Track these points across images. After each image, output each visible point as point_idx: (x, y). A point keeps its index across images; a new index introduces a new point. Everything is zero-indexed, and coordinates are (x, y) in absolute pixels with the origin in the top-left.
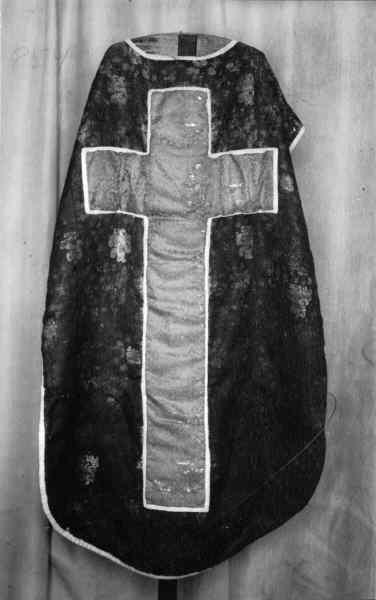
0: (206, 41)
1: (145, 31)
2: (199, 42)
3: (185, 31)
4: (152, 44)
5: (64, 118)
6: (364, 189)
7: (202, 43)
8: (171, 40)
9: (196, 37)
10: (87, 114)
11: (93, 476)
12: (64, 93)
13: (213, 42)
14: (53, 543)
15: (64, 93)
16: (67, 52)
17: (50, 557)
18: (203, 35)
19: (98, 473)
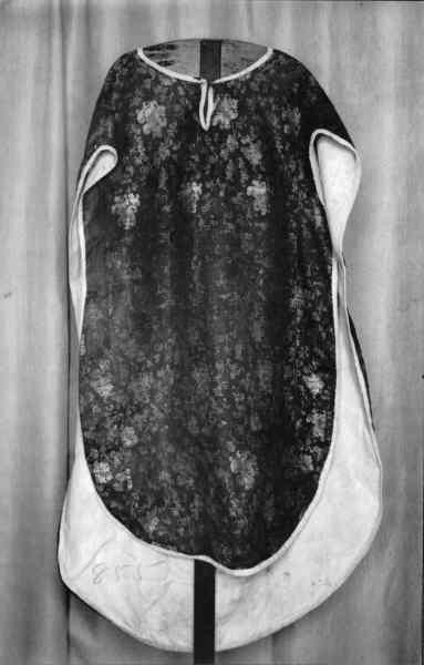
0: (231, 48)
1: (161, 38)
2: (223, 48)
3: (207, 37)
4: (169, 51)
5: (70, 89)
6: (313, 584)
7: (227, 50)
8: (192, 47)
9: (219, 43)
10: (93, 275)
11: (134, 217)
12: (70, 107)
13: (247, 52)
14: (71, 613)
15: (70, 107)
16: (77, 214)
17: (68, 638)
18: (227, 40)
19: (140, 214)
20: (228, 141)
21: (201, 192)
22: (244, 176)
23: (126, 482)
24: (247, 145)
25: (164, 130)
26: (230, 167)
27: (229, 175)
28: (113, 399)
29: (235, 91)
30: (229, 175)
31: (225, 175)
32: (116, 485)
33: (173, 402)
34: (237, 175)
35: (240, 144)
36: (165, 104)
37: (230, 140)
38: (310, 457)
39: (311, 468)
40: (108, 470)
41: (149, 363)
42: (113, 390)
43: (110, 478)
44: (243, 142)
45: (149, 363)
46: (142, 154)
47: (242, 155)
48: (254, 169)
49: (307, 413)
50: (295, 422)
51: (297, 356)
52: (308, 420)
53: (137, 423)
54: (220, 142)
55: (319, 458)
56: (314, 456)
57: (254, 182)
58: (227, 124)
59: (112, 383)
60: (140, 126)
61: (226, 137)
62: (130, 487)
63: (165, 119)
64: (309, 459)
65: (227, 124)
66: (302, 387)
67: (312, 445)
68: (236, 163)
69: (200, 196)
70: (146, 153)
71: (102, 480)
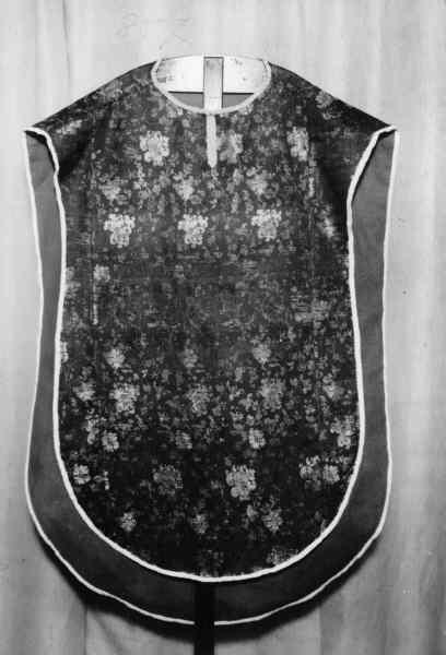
20: (235, 175)
21: (133, 226)
22: (176, 211)
23: (103, 483)
24: (252, 177)
25: (166, 159)
26: (236, 200)
27: (234, 208)
28: (95, 403)
29: (239, 127)
30: (234, 208)
31: (231, 209)
32: (93, 486)
33: (253, 413)
34: (242, 206)
35: (173, 181)
36: (241, 133)
37: (236, 174)
38: (336, 468)
39: (337, 478)
40: (86, 472)
41: (136, 376)
42: (95, 395)
43: (88, 480)
44: (248, 174)
45: (136, 376)
46: (141, 180)
47: (174, 191)
48: (185, 203)
49: (331, 422)
50: (319, 434)
51: (317, 367)
52: (332, 431)
53: (121, 430)
54: (227, 177)
55: (344, 469)
56: (340, 466)
57: (185, 216)
58: (234, 159)
59: (94, 389)
60: (142, 153)
61: (233, 171)
62: (107, 487)
63: (168, 150)
64: (334, 470)
65: (234, 159)
66: (323, 398)
67: (337, 456)
68: (168, 198)
69: (280, 223)
70: (219, 177)
71: (81, 481)
